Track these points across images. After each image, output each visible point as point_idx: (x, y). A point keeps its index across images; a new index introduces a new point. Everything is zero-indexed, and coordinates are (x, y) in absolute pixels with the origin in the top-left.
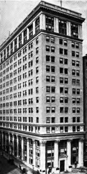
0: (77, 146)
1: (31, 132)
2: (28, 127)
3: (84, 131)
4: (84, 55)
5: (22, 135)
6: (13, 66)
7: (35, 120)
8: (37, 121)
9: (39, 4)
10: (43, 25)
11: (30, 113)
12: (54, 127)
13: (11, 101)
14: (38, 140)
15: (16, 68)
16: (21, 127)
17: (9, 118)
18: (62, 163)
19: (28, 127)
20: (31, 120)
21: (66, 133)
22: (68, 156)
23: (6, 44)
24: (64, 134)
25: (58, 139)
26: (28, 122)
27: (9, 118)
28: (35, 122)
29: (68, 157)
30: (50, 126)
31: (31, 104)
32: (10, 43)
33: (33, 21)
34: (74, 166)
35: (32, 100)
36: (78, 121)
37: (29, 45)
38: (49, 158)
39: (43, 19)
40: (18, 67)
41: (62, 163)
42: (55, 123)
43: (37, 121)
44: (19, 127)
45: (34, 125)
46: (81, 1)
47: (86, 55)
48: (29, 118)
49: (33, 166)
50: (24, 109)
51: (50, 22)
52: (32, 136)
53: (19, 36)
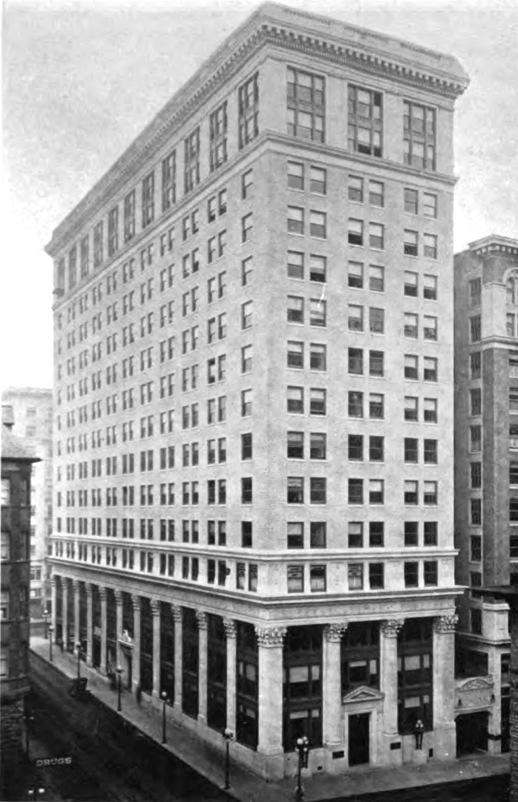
0: (427, 650)
1: (189, 580)
2: (203, 567)
3: (457, 583)
4: (460, 245)
5: (137, 591)
6: (137, 297)
7: (234, 532)
8: (247, 541)
9: (226, 46)
10: (274, 113)
11: (111, 506)
12: (325, 566)
13: (145, 448)
14: (219, 613)
15: (152, 306)
16: (99, 557)
17: (120, 526)
18: (359, 727)
19: (203, 567)
20: (128, 524)
21: (375, 591)
22: (383, 695)
23: (183, 117)
24: (365, 595)
25: (339, 618)
26: (202, 545)
27: (120, 526)
28: (233, 545)
29: (386, 699)
30: (306, 560)
31: (147, 471)
32: (210, 107)
33: (229, 94)
34: (408, 740)
35: (196, 448)
36: (431, 539)
37: (184, 221)
38: (296, 704)
39: (274, 78)
40: (158, 299)
41: (359, 727)
42: (324, 546)
43: (247, 541)
44: (108, 559)
45: (232, 556)
46: (54, 308)
47: (467, 248)
48: (80, 519)
49: (227, 737)
50: (143, 487)
51: (307, 100)
52: (169, 594)
53: (146, 181)
